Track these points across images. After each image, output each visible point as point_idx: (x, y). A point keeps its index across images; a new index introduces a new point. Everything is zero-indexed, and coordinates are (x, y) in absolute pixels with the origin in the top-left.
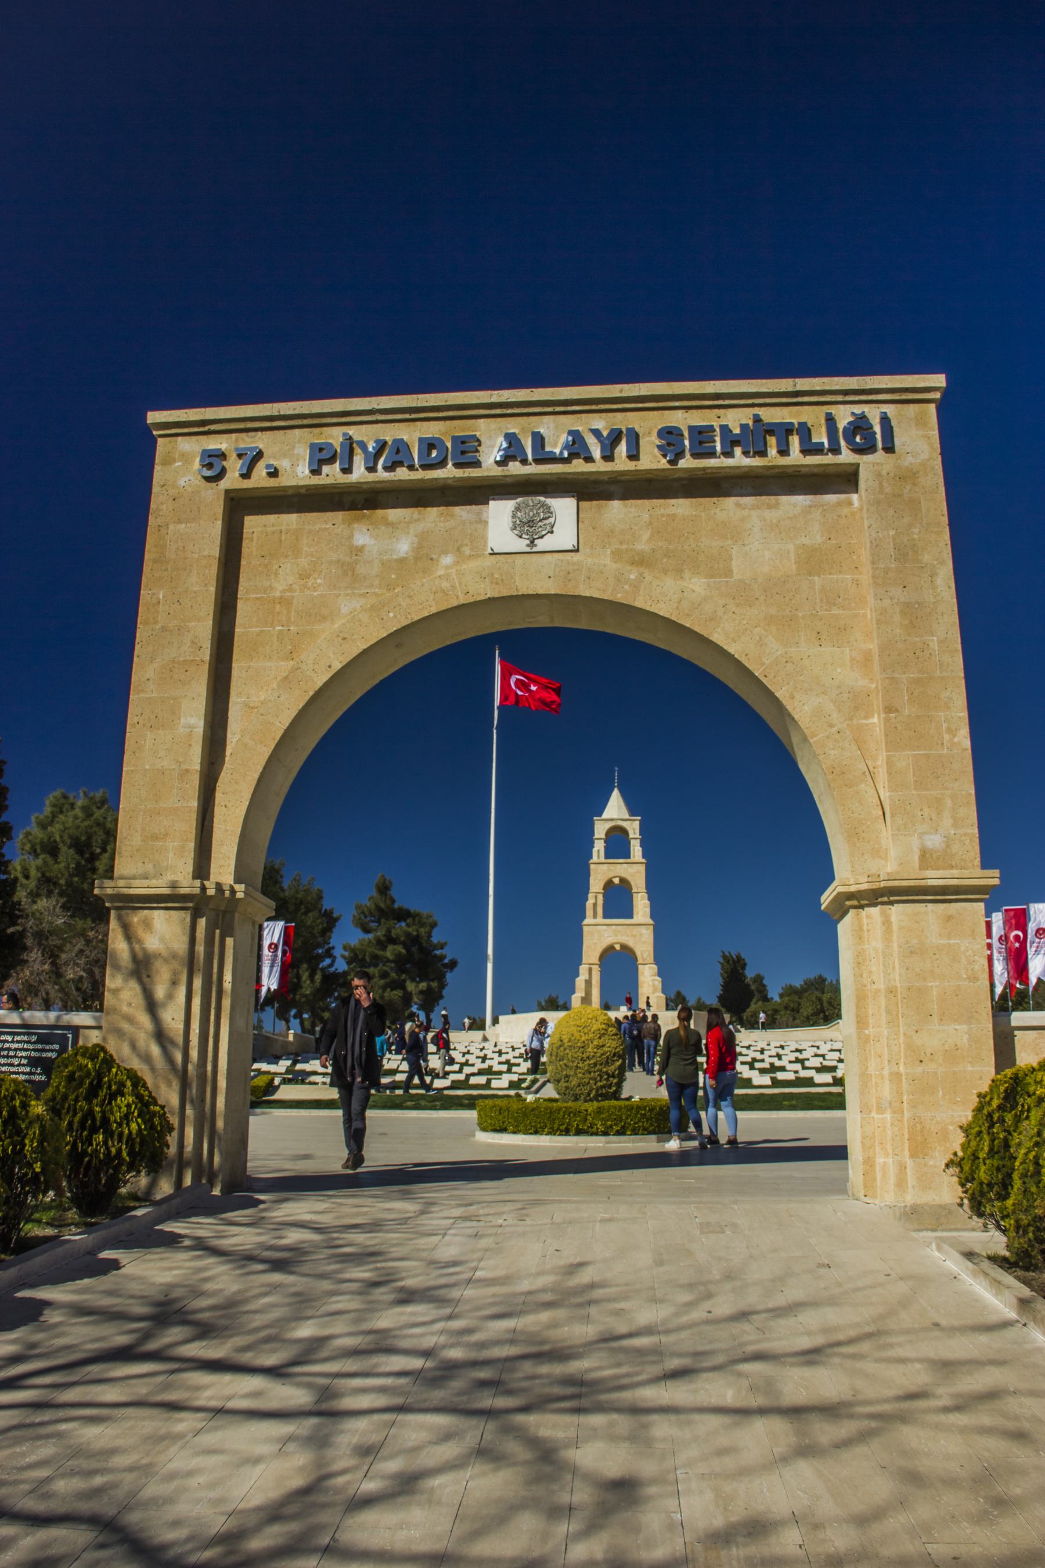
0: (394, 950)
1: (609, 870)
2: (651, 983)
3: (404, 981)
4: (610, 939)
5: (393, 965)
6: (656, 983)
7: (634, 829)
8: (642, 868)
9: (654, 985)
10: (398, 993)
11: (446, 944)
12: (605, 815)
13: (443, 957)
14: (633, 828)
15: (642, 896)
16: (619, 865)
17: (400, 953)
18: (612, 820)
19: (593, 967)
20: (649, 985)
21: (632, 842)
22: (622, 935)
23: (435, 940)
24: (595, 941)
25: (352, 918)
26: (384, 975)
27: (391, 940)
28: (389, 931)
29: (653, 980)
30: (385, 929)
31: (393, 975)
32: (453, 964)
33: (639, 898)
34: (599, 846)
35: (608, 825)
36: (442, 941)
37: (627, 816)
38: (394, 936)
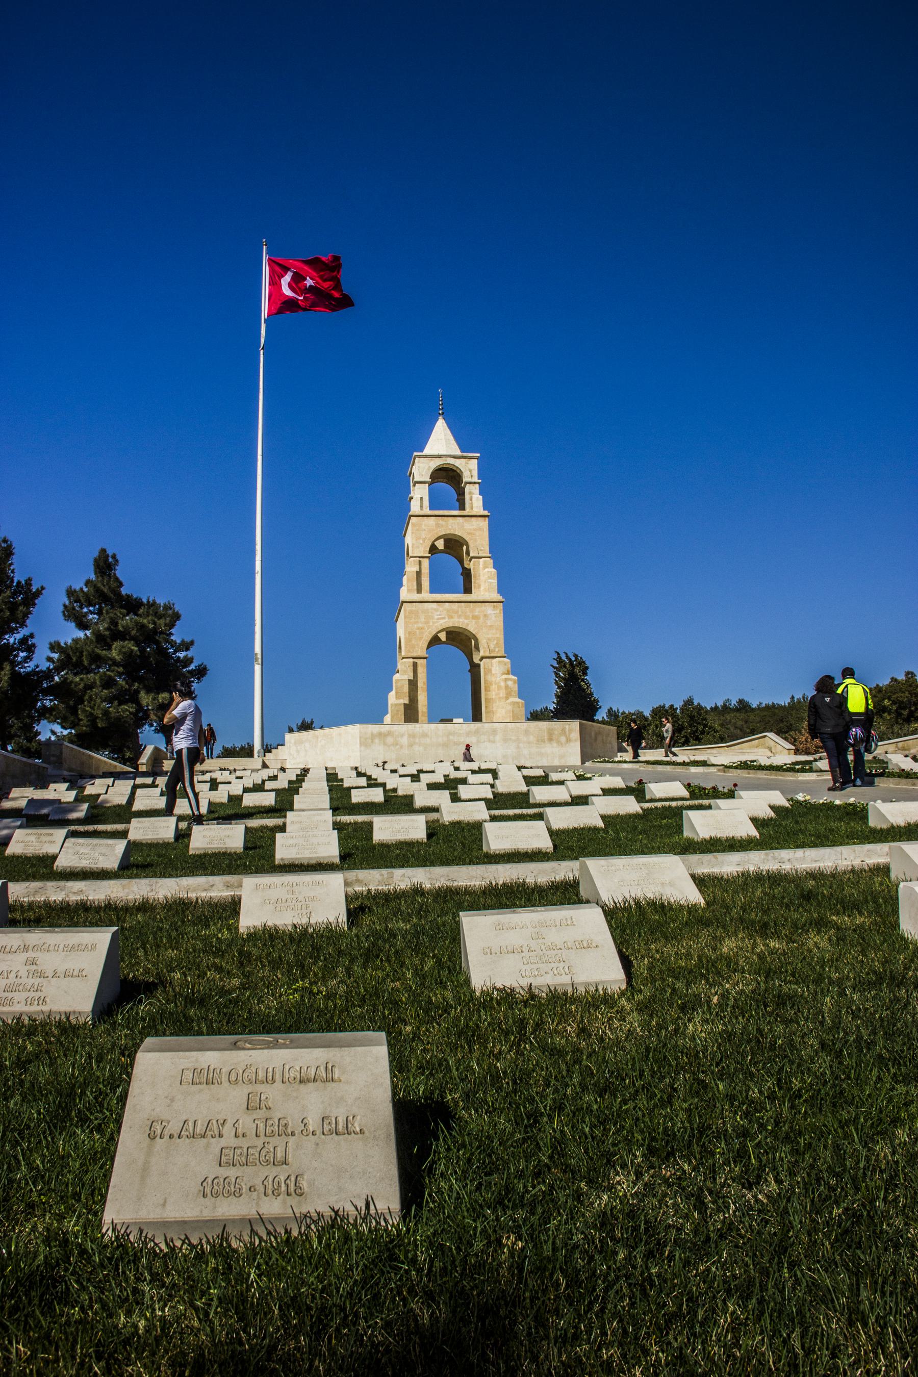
0: (123, 647)
1: (438, 525)
2: (503, 684)
3: (137, 692)
4: (442, 621)
5: (121, 669)
6: (510, 683)
7: (470, 471)
8: (484, 524)
9: (507, 687)
10: (129, 708)
11: (192, 643)
12: (427, 451)
13: (188, 661)
14: (469, 469)
15: (485, 562)
16: (451, 520)
17: (132, 651)
18: (440, 456)
19: (419, 661)
20: (499, 688)
21: (468, 488)
22: (459, 617)
23: (176, 638)
24: (420, 625)
25: (62, 608)
26: (108, 683)
27: (118, 635)
28: (114, 623)
29: (506, 680)
30: (108, 620)
31: (120, 681)
32: (201, 672)
33: (481, 566)
34: (419, 495)
35: (435, 464)
36: (188, 639)
37: (458, 452)
38: (121, 629)
